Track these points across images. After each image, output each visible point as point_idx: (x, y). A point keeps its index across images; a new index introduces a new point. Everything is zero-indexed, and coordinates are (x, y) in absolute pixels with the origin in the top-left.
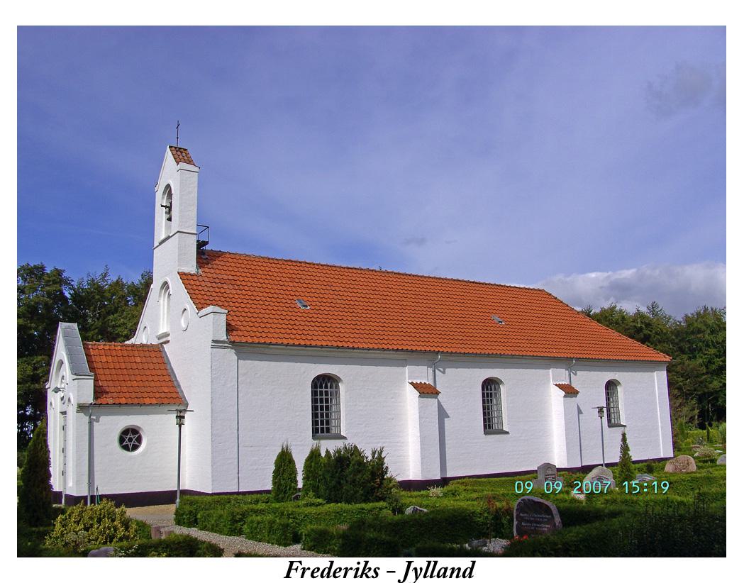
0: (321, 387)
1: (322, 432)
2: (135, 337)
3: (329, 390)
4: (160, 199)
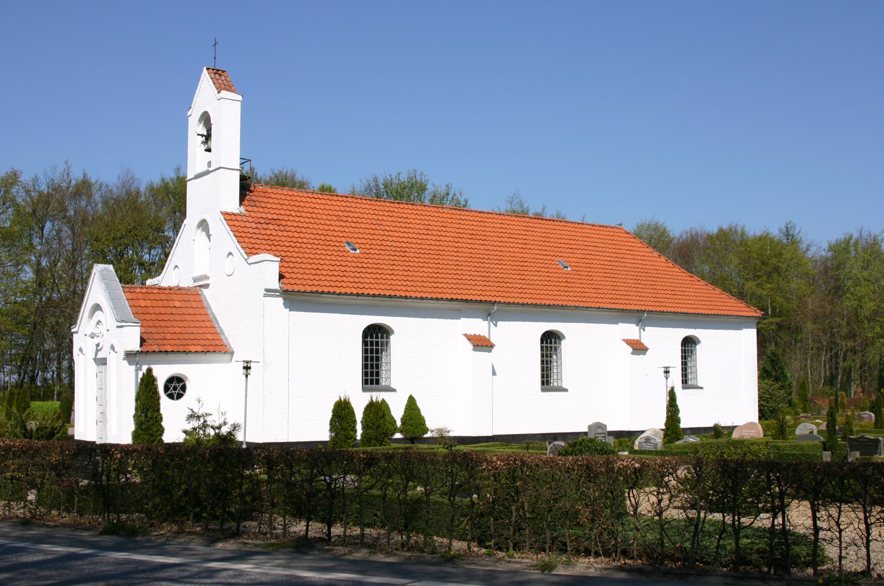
0: (372, 337)
1: (372, 383)
2: (161, 275)
3: (374, 340)
4: (195, 128)
